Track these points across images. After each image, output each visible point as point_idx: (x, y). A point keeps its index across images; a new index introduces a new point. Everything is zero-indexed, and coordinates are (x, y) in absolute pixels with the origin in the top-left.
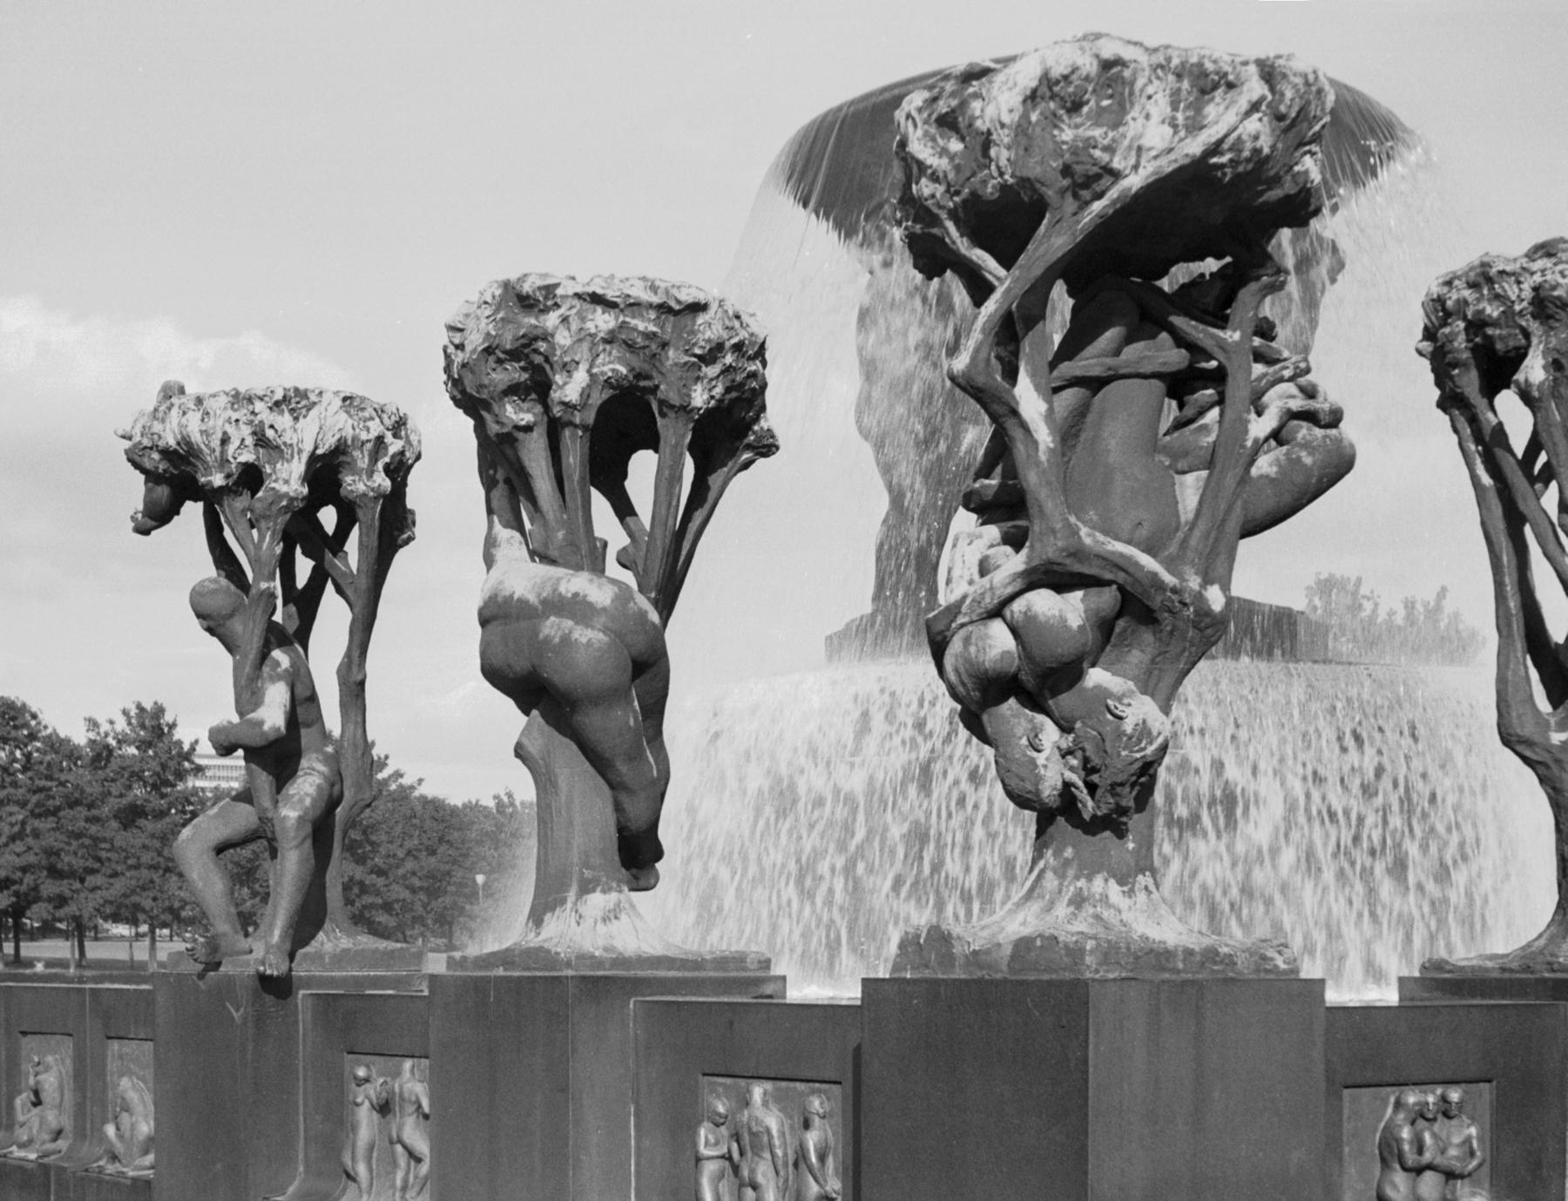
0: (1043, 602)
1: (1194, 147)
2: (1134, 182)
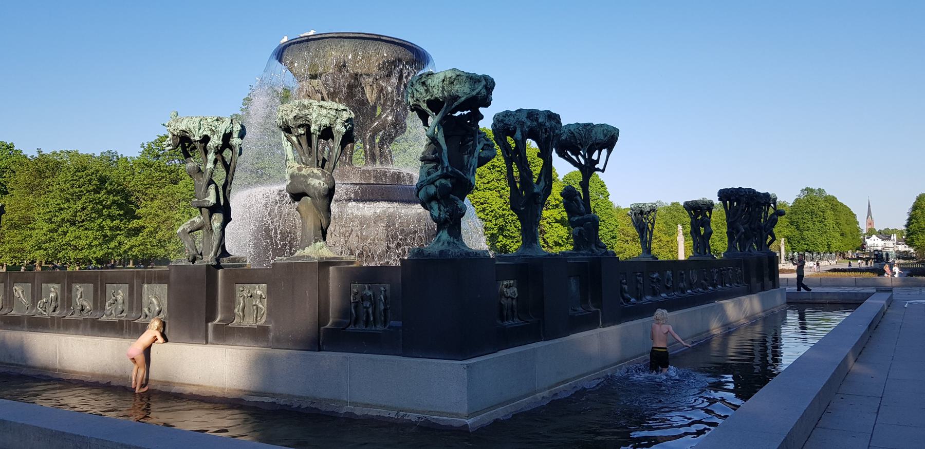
0: (443, 181)
1: (474, 93)
2: (463, 99)
